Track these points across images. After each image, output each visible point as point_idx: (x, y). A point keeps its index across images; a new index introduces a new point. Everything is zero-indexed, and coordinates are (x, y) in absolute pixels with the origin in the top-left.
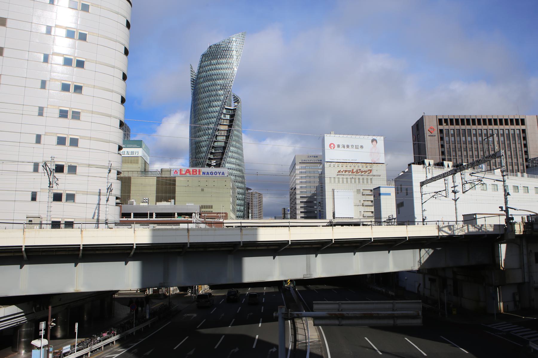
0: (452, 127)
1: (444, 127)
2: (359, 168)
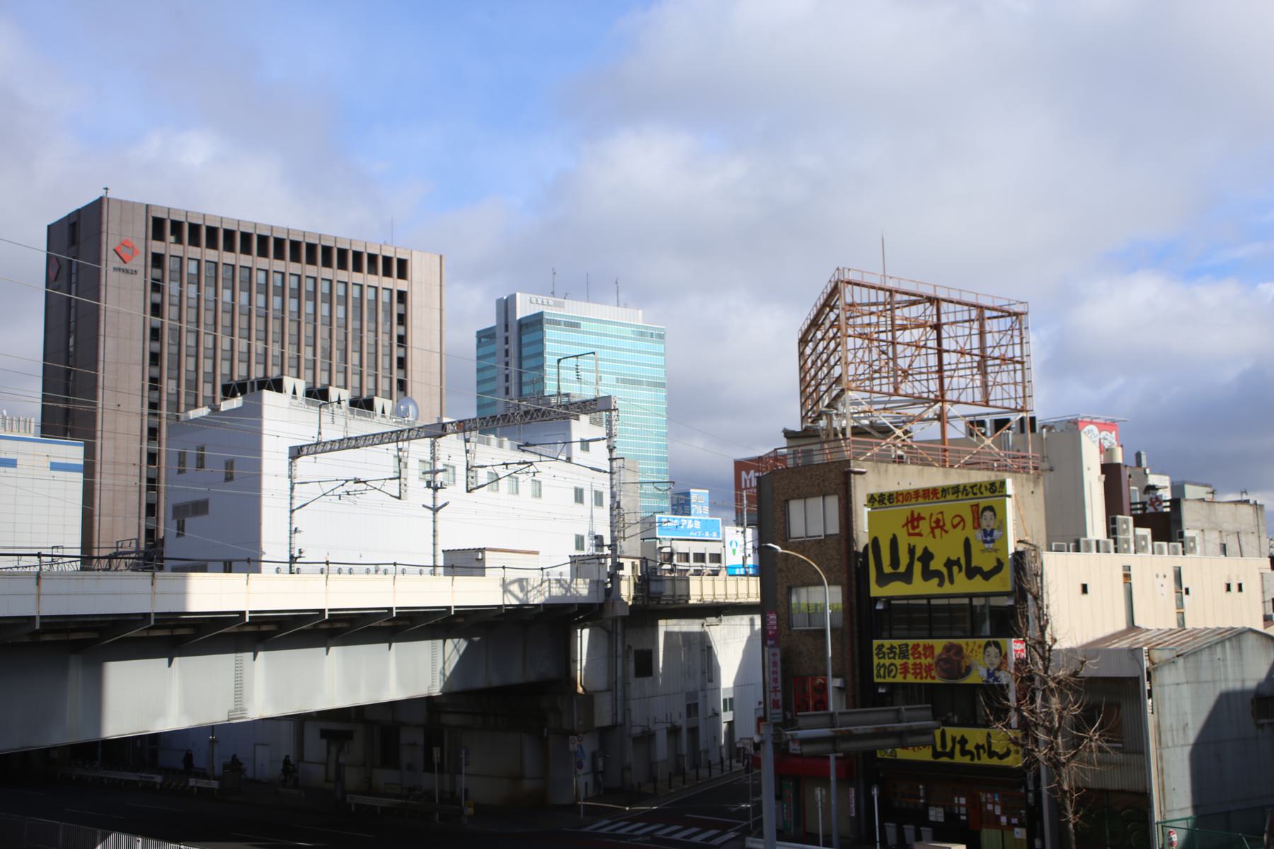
1: (169, 247)
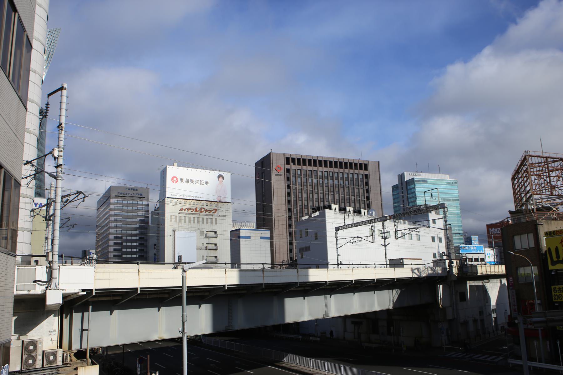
0: (299, 167)
1: (291, 166)
2: (203, 207)
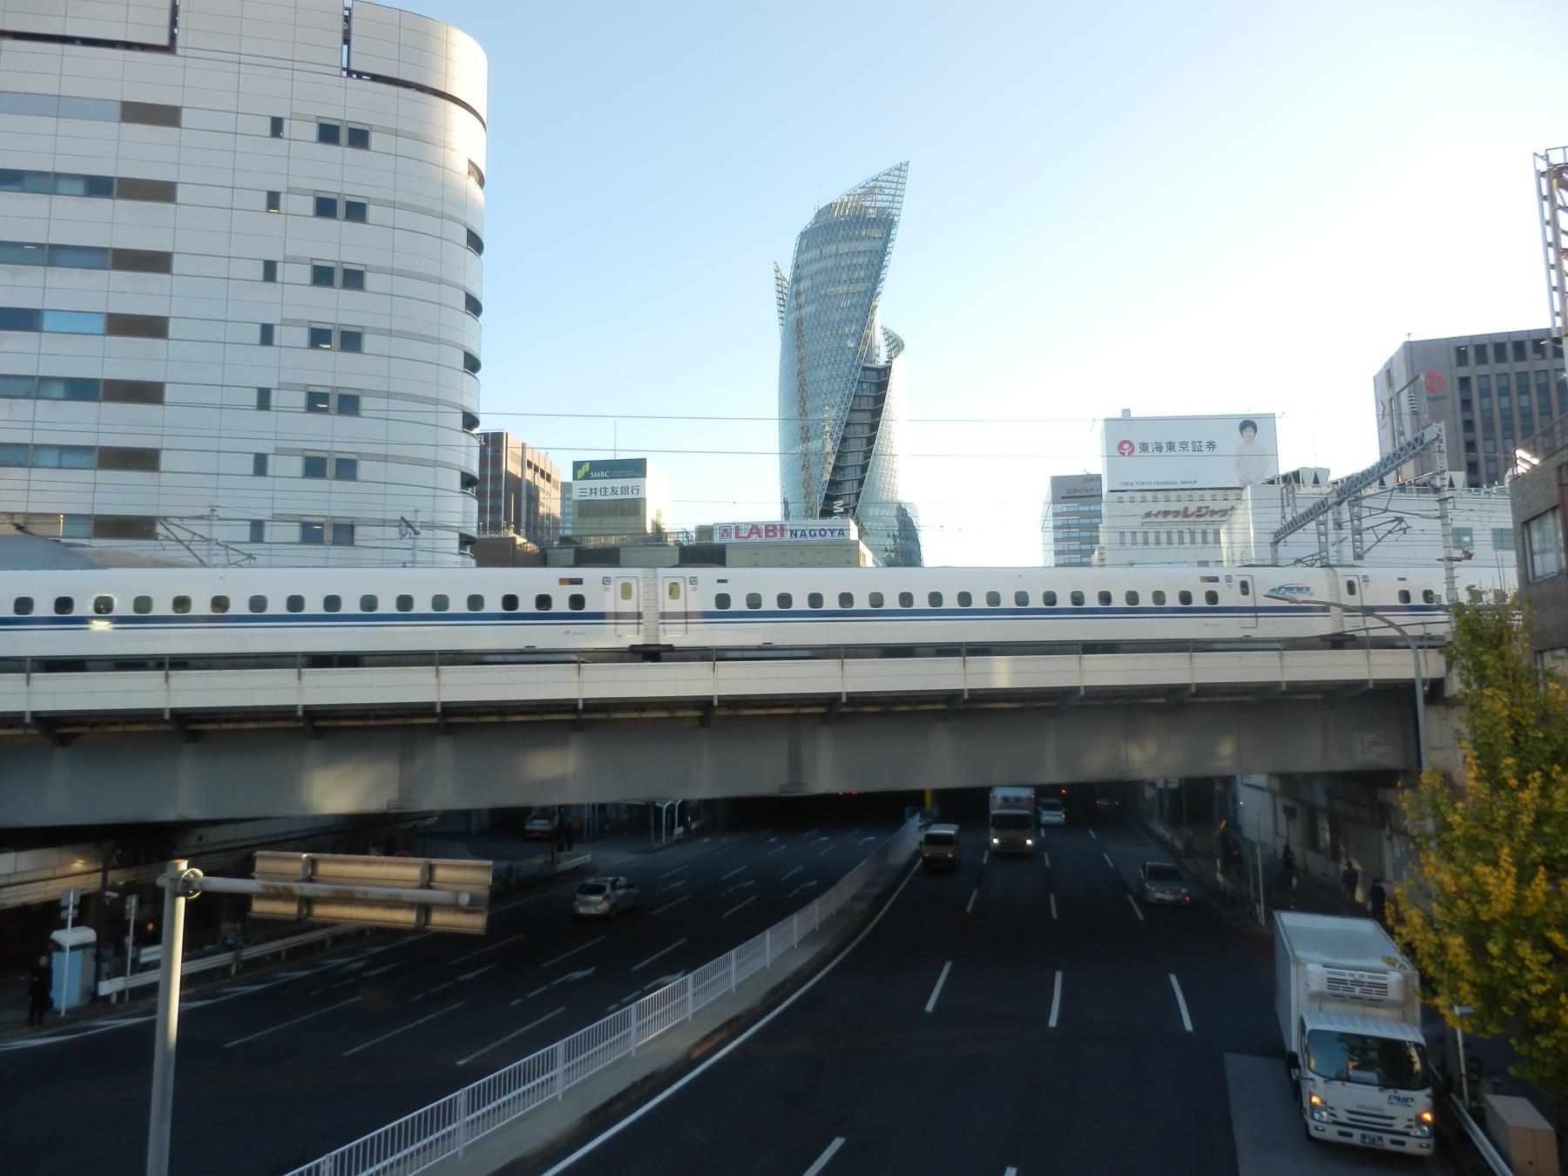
1: (1472, 370)
2: (1202, 504)
